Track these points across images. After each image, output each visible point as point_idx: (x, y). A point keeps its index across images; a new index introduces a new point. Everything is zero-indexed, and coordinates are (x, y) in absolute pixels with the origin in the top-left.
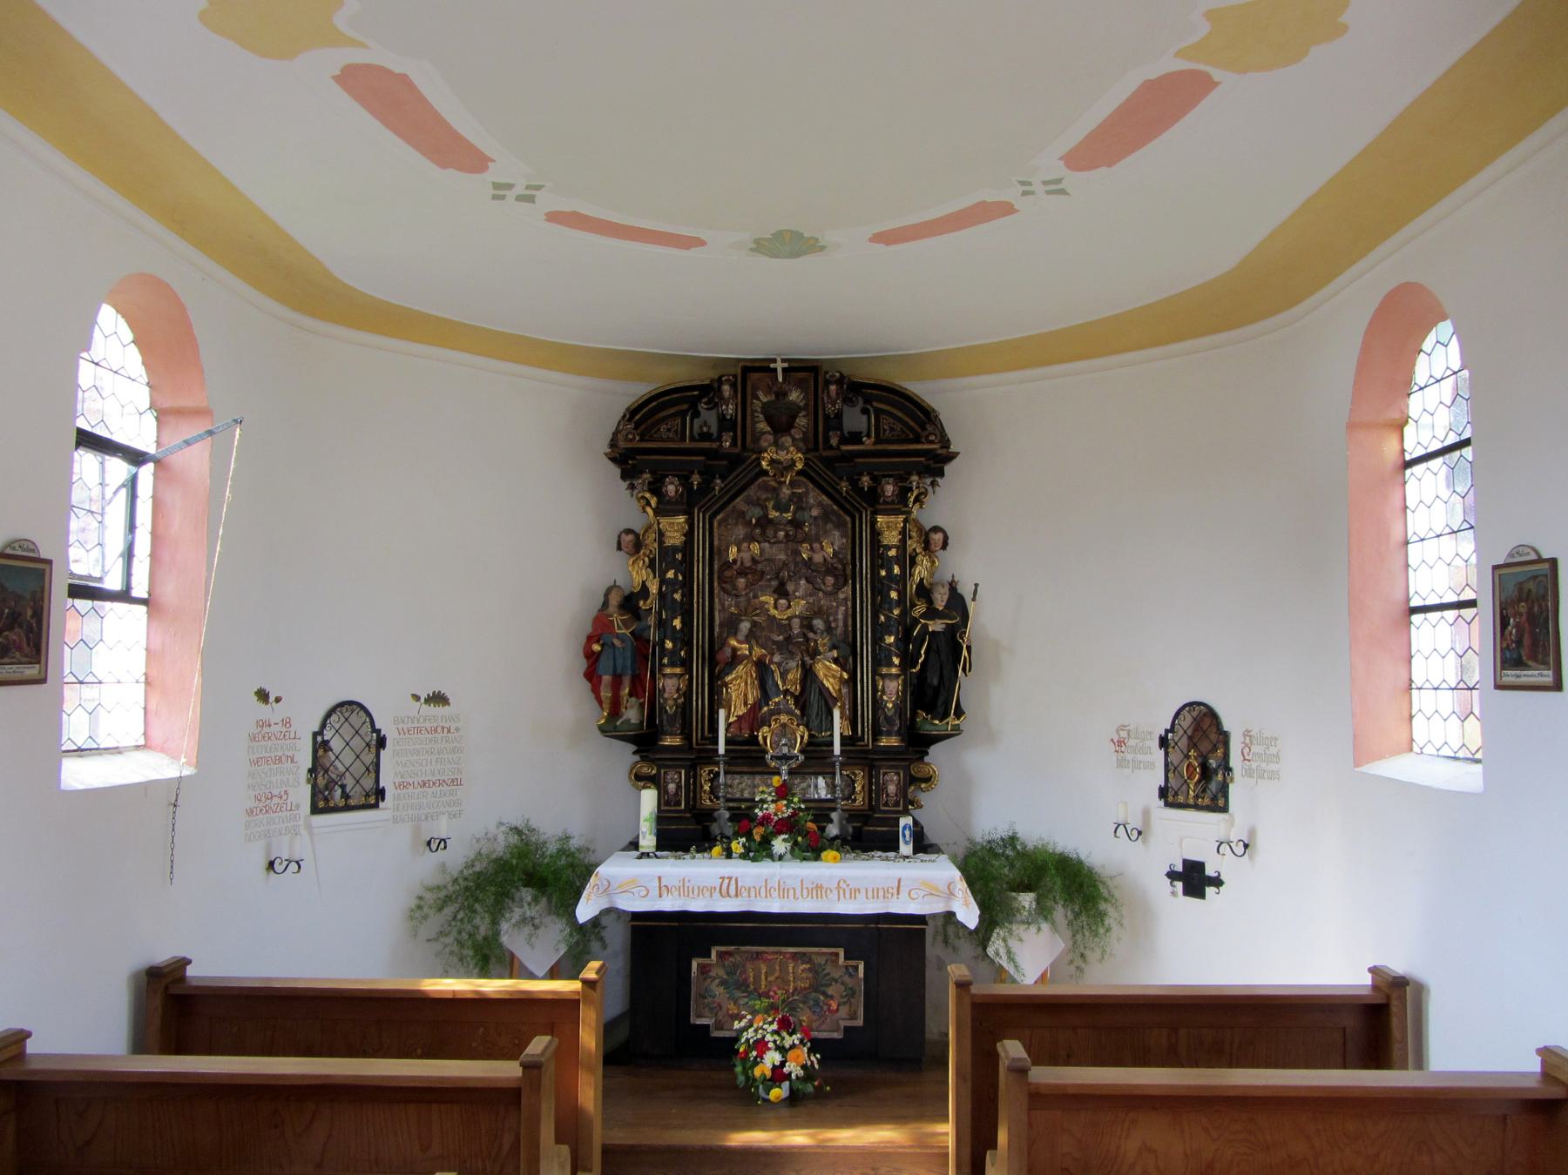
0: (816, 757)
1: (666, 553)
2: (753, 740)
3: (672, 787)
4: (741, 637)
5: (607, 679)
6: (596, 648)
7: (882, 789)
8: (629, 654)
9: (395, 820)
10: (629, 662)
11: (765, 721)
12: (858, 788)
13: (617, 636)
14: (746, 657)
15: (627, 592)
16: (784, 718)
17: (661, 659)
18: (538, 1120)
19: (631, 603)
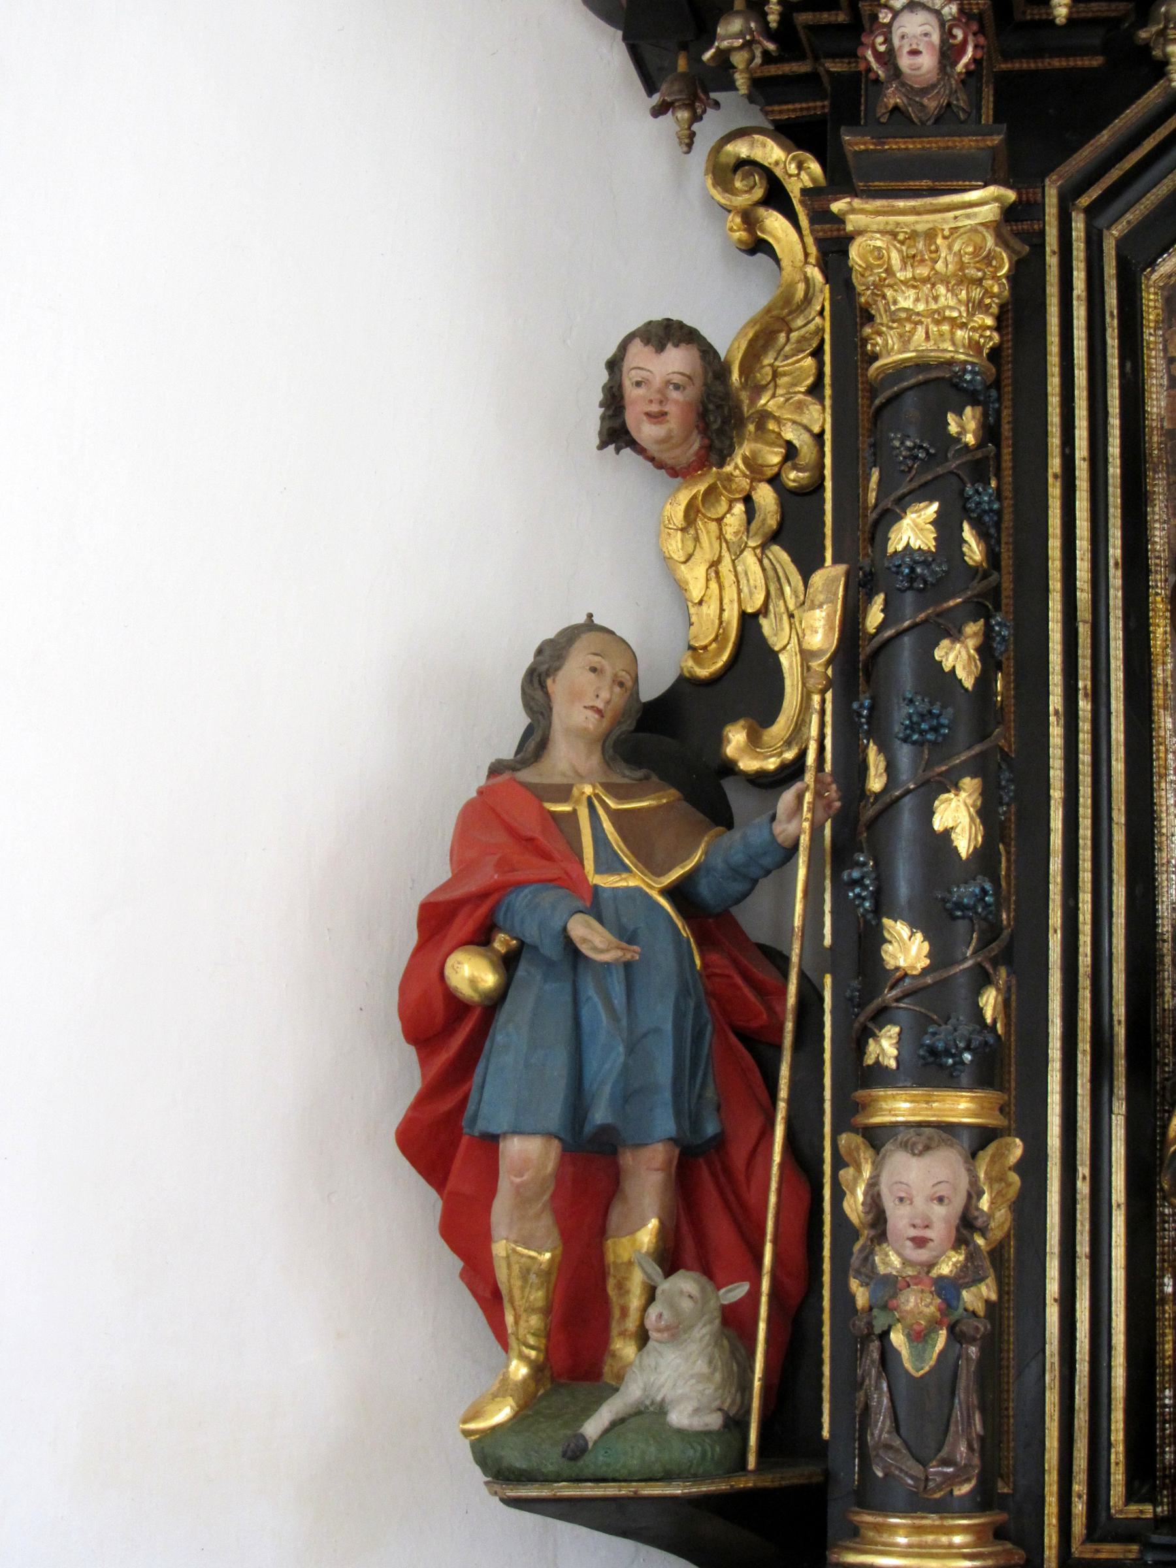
1: (877, 409)
5: (527, 1156)
6: (471, 973)
8: (660, 1012)
10: (663, 1069)
13: (596, 905)
15: (653, 685)
17: (855, 1041)
18: (1104, 330)
19: (672, 736)
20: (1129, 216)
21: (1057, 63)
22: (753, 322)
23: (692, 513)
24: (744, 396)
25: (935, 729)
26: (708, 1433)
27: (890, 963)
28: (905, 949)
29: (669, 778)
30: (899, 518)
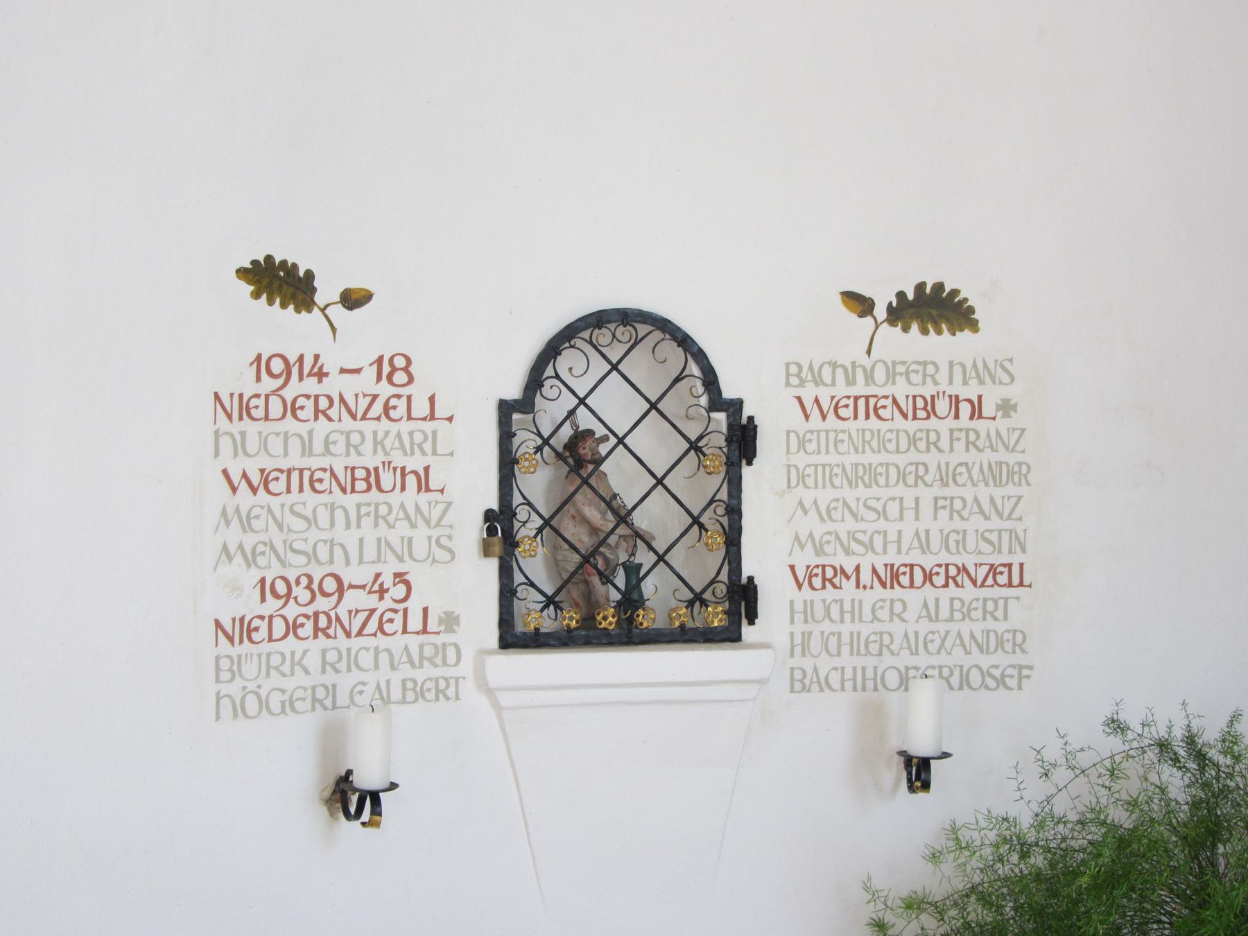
9: (800, 683)
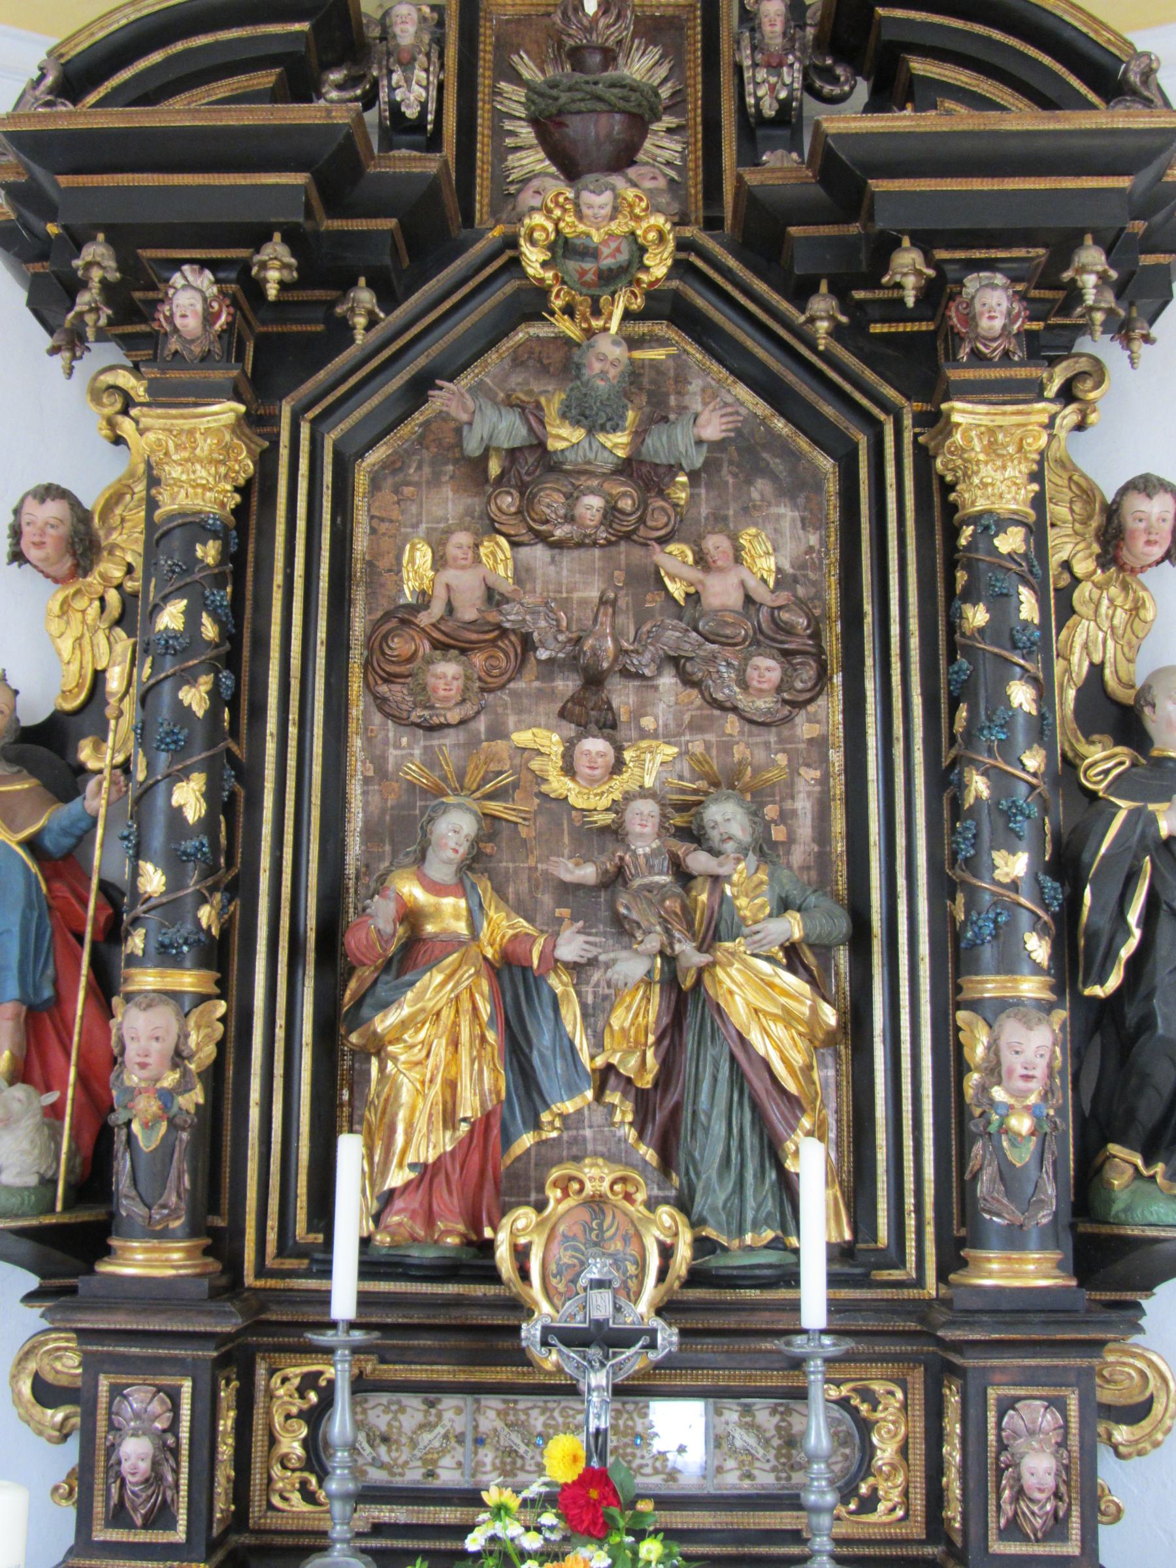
0: (722, 1320)
2: (476, 1261)
3: (135, 1452)
4: (441, 868)
7: (989, 1467)
11: (523, 1186)
12: (885, 1452)
14: (452, 943)
16: (597, 1176)
20: (342, 426)
21: (295, 328)
22: (109, 488)
23: (65, 605)
24: (101, 533)
25: (175, 742)
26: (27, 1188)
27: (141, 890)
28: (151, 881)
29: (33, 772)
30: (162, 609)
